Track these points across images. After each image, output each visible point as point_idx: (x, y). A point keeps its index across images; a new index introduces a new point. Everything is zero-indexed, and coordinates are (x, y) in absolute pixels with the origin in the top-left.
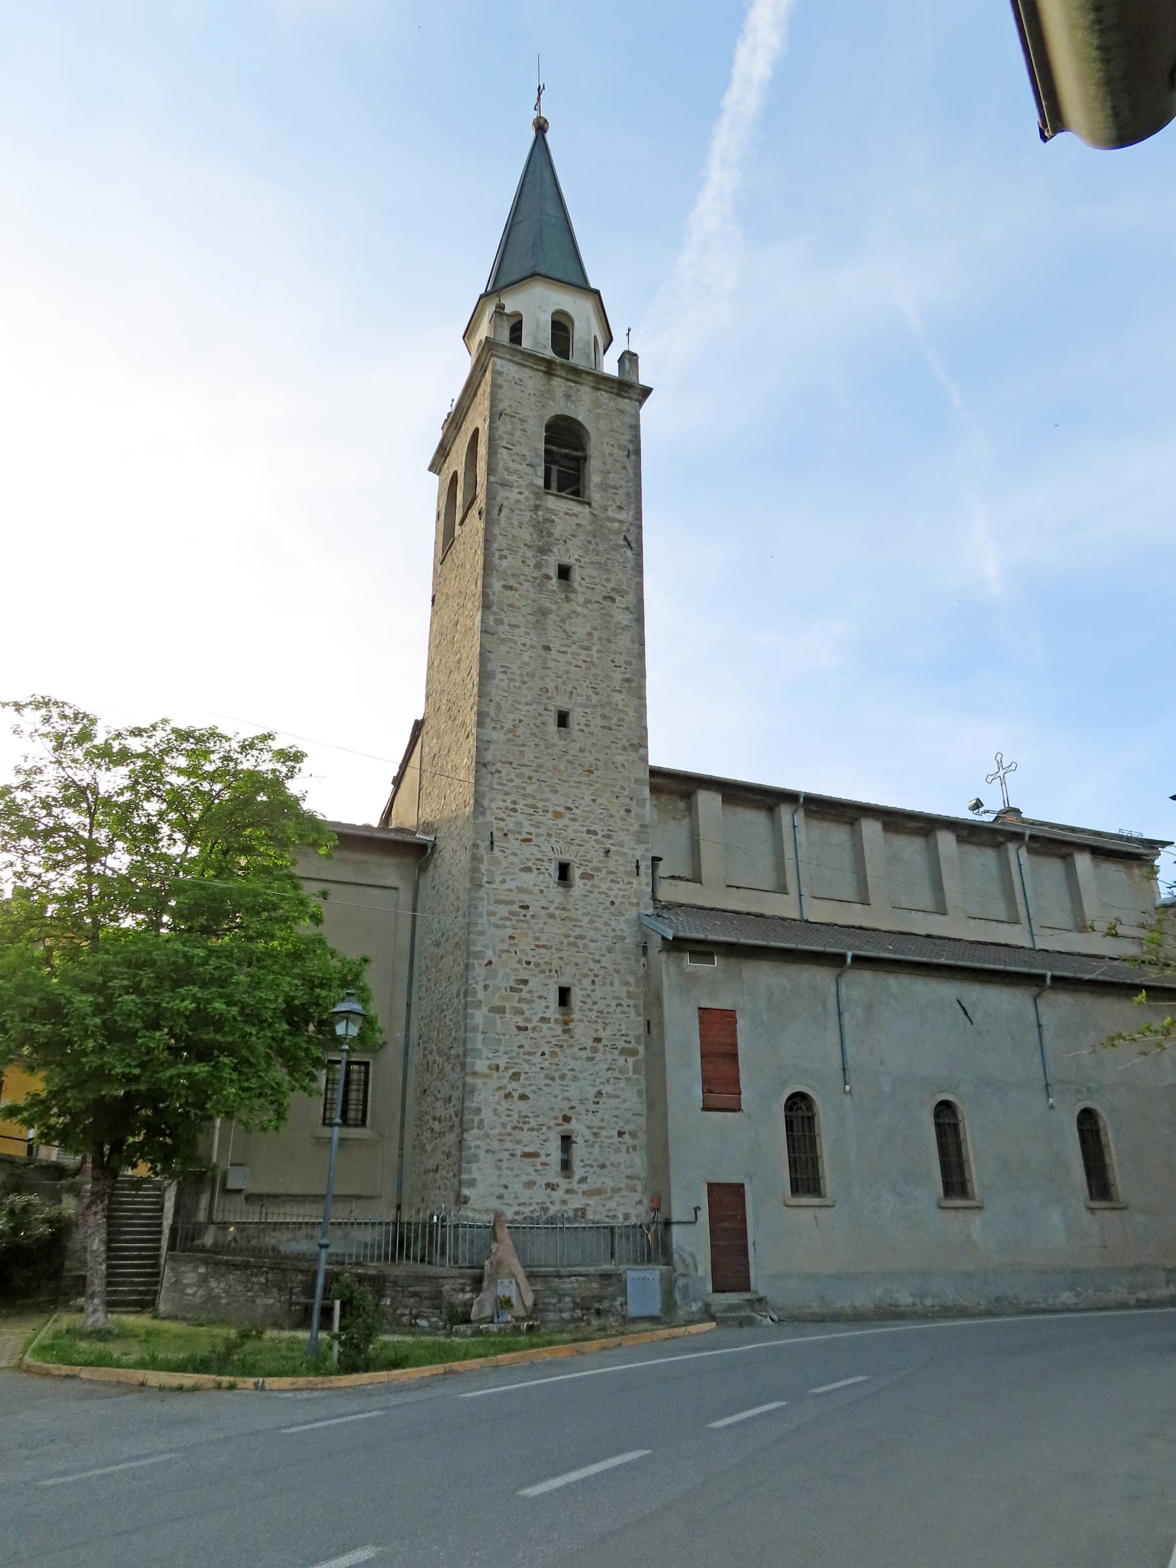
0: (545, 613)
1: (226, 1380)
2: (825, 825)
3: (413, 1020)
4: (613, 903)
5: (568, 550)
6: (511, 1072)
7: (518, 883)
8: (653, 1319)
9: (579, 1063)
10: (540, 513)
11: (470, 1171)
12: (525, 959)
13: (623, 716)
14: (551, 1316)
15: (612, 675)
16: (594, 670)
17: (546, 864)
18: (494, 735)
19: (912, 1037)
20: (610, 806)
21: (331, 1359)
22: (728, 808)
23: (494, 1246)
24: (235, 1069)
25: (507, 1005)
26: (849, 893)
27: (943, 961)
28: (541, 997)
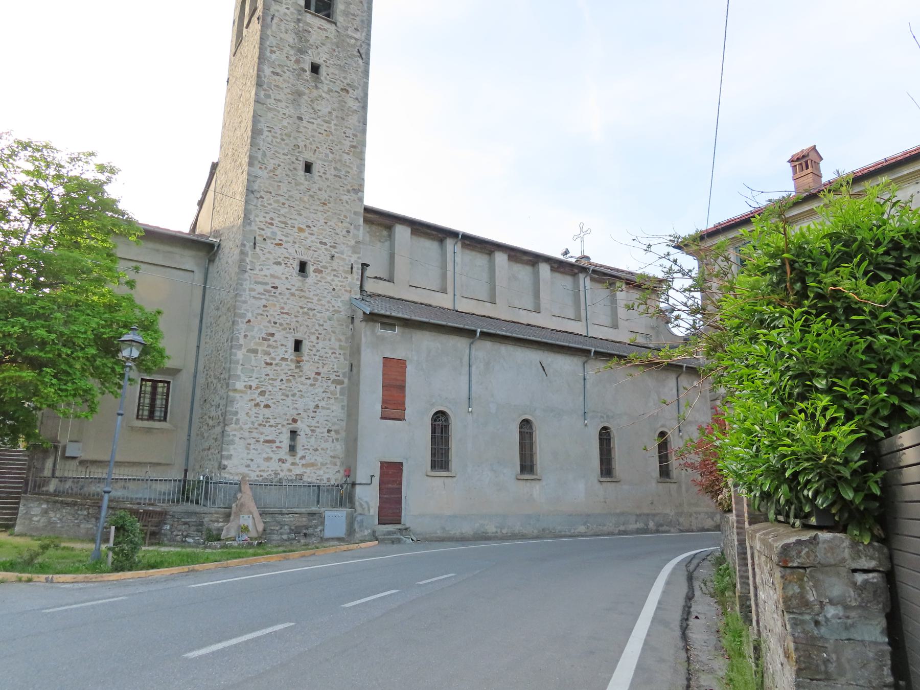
0: (300, 94)
1: (25, 576)
2: (474, 253)
3: (201, 357)
4: (334, 289)
5: (319, 54)
6: (259, 390)
7: (271, 271)
8: (340, 539)
9: (305, 387)
10: (301, 25)
11: (228, 450)
12: (273, 320)
13: (348, 169)
14: (275, 537)
15: (344, 142)
16: (331, 137)
17: (291, 261)
18: (259, 173)
19: (513, 381)
20: (336, 228)
21: (106, 564)
22: (415, 238)
23: (239, 495)
24: (55, 376)
25: (260, 349)
26: (484, 295)
27: (533, 338)
28: (282, 345)
